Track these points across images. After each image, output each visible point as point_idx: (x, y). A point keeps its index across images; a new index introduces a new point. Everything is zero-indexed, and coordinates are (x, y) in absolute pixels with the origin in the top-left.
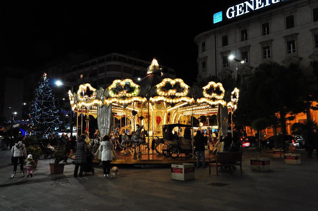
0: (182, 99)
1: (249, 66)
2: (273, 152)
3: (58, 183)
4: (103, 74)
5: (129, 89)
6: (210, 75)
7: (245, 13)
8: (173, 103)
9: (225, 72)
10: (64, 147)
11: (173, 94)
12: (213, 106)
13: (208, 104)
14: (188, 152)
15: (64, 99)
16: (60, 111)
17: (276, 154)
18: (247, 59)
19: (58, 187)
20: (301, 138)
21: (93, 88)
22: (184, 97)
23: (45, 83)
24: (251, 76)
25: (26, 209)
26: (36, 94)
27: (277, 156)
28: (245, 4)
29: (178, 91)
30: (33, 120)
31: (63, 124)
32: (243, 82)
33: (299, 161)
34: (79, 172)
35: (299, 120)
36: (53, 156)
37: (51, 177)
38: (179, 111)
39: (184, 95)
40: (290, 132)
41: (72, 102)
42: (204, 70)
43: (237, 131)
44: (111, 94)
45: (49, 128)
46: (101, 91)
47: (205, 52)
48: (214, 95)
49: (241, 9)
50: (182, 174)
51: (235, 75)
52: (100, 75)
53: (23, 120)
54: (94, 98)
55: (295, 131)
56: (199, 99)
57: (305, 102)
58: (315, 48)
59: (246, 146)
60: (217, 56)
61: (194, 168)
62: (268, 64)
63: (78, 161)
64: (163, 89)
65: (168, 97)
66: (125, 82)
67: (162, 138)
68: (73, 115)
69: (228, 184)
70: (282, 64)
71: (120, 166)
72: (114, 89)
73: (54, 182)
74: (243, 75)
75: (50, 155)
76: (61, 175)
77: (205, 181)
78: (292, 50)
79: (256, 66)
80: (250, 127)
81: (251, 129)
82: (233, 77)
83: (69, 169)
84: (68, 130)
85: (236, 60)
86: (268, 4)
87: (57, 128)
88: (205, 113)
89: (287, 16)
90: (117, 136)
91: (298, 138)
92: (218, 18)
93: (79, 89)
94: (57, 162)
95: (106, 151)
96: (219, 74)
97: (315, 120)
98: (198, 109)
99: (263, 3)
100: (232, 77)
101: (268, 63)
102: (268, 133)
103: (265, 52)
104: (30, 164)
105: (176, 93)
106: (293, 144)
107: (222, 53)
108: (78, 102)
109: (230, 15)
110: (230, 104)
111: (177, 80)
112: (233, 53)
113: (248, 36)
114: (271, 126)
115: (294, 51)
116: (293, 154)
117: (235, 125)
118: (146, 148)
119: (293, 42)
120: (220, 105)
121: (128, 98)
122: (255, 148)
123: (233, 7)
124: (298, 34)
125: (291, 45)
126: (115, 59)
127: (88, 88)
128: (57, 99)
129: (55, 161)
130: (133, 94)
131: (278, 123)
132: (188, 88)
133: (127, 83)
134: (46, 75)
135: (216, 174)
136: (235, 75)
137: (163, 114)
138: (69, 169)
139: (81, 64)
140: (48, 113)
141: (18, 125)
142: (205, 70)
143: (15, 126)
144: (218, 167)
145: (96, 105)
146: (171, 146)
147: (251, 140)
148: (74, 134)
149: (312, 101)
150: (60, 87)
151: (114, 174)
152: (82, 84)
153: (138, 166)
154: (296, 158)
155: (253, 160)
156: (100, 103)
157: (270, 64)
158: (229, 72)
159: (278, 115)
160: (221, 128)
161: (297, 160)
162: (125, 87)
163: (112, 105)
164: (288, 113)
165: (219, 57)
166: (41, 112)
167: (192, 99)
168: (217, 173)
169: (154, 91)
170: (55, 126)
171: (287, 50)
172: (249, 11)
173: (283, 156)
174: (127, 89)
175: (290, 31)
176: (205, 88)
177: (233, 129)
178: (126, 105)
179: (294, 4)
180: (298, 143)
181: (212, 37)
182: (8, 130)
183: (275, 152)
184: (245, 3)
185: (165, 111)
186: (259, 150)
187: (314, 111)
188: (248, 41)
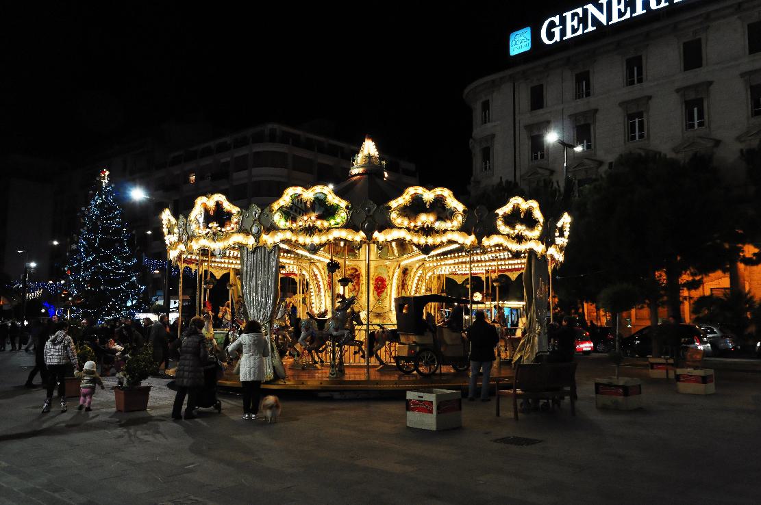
0: (450, 236)
2: (650, 365)
4: (244, 174)
6: (501, 178)
7: (585, 31)
8: (427, 245)
11: (428, 225)
12: (517, 255)
13: (506, 249)
14: (459, 362)
15: (149, 232)
16: (140, 260)
17: (655, 371)
18: (589, 141)
20: (715, 333)
21: (232, 205)
22: (452, 233)
25: (57, 495)
27: (657, 373)
28: (587, 9)
29: (439, 218)
30: (74, 281)
33: (711, 388)
34: (184, 407)
37: (118, 420)
38: (427, 265)
39: (453, 227)
40: (690, 316)
41: (169, 239)
44: (278, 219)
46: (253, 213)
47: (489, 125)
48: (520, 228)
49: (575, 23)
51: (560, 181)
52: (236, 175)
53: (51, 282)
54: (235, 229)
56: (488, 237)
58: (752, 117)
59: (585, 349)
60: (517, 132)
61: (459, 401)
62: (640, 155)
63: (185, 380)
65: (417, 232)
66: (313, 193)
67: (396, 327)
68: (170, 272)
70: (673, 155)
71: (284, 395)
73: (125, 430)
74: (579, 181)
76: (140, 414)
78: (696, 122)
79: (611, 158)
80: (594, 305)
81: (598, 309)
82: (555, 185)
83: (161, 396)
84: (159, 305)
85: (565, 145)
86: (640, 11)
88: (481, 272)
90: (285, 322)
92: (520, 43)
95: (252, 358)
96: (521, 177)
98: (479, 259)
99: (629, 8)
100: (553, 183)
101: (639, 151)
102: (637, 318)
103: (633, 125)
104: (90, 381)
105: (435, 222)
106: (696, 347)
107: (529, 128)
108: (191, 237)
109: (550, 35)
110: (552, 251)
111: (439, 191)
112: (556, 127)
113: (591, 87)
114: (645, 303)
115: (701, 124)
116: (696, 371)
117: (559, 299)
118: (355, 353)
119: (699, 103)
120: (532, 252)
121: (320, 231)
122: (606, 354)
123: (558, 16)
124: (711, 83)
125: (696, 110)
126: (273, 138)
127: (218, 205)
128: (134, 232)
130: (332, 222)
131: (662, 296)
132: (464, 211)
134: (107, 173)
135: (511, 415)
136: (560, 181)
137: (391, 274)
138: (161, 396)
140: (111, 265)
142: (489, 167)
143: (30, 296)
144: (518, 400)
145: (241, 247)
146: (418, 349)
147: (597, 335)
149: (744, 243)
150: (140, 203)
151: (268, 413)
152: (204, 194)
154: (704, 380)
155: (601, 384)
156: (250, 241)
157: (643, 154)
158: (547, 173)
159: (662, 276)
160: (533, 308)
163: (280, 249)
164: (686, 272)
166: (93, 263)
167: (472, 238)
170: (127, 298)
172: (595, 28)
173: (672, 375)
174: (318, 210)
176: (500, 212)
177: (554, 309)
178: (315, 248)
179: (703, 11)
180: (709, 345)
181: (507, 88)
183: (652, 366)
184: (585, 7)
185: (396, 263)
187: (748, 267)
188: (591, 99)
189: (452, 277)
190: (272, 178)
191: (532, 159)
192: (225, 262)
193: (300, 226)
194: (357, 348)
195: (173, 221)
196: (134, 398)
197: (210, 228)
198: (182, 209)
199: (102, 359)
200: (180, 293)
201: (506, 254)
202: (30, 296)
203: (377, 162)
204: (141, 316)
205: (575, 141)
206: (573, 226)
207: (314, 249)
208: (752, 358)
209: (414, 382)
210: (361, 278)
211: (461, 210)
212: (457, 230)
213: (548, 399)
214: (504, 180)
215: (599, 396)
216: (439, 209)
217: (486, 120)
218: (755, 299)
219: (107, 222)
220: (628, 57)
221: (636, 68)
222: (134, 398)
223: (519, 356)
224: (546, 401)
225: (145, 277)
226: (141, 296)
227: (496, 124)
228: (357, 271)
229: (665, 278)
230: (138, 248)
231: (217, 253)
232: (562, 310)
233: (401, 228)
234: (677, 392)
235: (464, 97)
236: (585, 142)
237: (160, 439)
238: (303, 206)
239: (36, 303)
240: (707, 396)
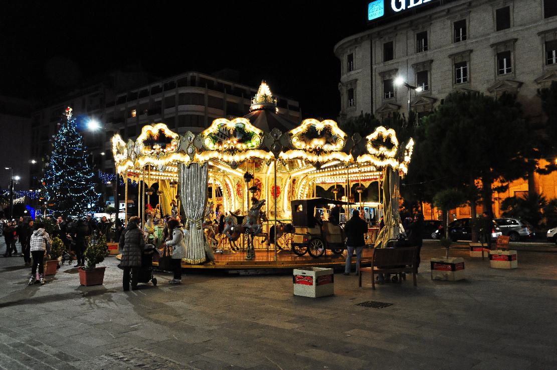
0: (334, 155)
1: (430, 96)
3: (94, 303)
4: (173, 109)
5: (242, 135)
6: (362, 112)
9: (387, 108)
11: (319, 148)
12: (380, 169)
15: (103, 154)
17: (475, 252)
20: (517, 224)
21: (172, 132)
22: (336, 153)
23: (70, 124)
24: (433, 115)
25: (36, 348)
26: (54, 144)
27: (477, 254)
29: (327, 142)
32: (419, 125)
33: (515, 264)
35: (515, 192)
37: (81, 292)
40: (499, 212)
41: (117, 158)
42: (351, 104)
43: (407, 210)
44: (208, 143)
45: (78, 205)
46: (189, 138)
47: (352, 72)
48: (383, 150)
50: (310, 287)
51: (405, 113)
53: (31, 191)
55: (507, 211)
61: (332, 276)
62: (464, 94)
63: (131, 262)
64: (303, 138)
65: (311, 152)
66: (235, 123)
67: (289, 222)
69: (392, 304)
73: (87, 299)
76: (98, 288)
77: (352, 299)
79: (443, 96)
80: (430, 205)
81: (432, 207)
82: (402, 116)
85: (409, 87)
89: (497, 9)
91: (513, 222)
96: (376, 111)
97: (543, 191)
100: (400, 115)
101: (463, 91)
102: (462, 212)
103: (459, 71)
107: (383, 74)
113: (428, 44)
114: (466, 203)
115: (508, 71)
117: (404, 201)
118: (263, 242)
119: (507, 55)
120: (389, 168)
121: (240, 151)
124: (516, 40)
125: (505, 60)
126: (193, 83)
128: (91, 154)
130: (249, 145)
132: (345, 137)
135: (370, 285)
136: (405, 113)
137: (284, 181)
139: (134, 91)
140: (75, 178)
145: (179, 164)
146: (310, 238)
148: (122, 216)
149: (539, 158)
154: (510, 258)
156: (186, 159)
157: (466, 93)
158: (395, 108)
161: (512, 262)
162: (235, 131)
165: (378, 82)
166: (62, 176)
169: (288, 141)
170: (88, 201)
171: (496, 69)
174: (239, 136)
175: (503, 35)
181: (366, 45)
183: (472, 249)
185: (287, 175)
186: (446, 244)
188: (428, 52)
189: (321, 185)
190: (194, 113)
191: (384, 98)
192: (374, 175)
193: (225, 148)
195: (123, 143)
196: (94, 277)
197: (154, 149)
198: (130, 134)
199: (70, 247)
201: (372, 168)
202: (17, 200)
203: (271, 101)
204: (98, 216)
205: (417, 83)
206: (415, 148)
207: (235, 166)
208: (543, 242)
209: (304, 262)
211: (343, 137)
213: (396, 274)
214: (364, 113)
215: (433, 270)
216: (327, 135)
218: (546, 199)
219: (71, 147)
220: (456, 21)
221: (461, 30)
223: (380, 242)
224: (395, 275)
225: (101, 187)
227: (358, 71)
228: (259, 181)
231: (159, 168)
233: (300, 150)
234: (490, 267)
235: (335, 51)
236: (424, 85)
237: (112, 306)
240: (512, 270)
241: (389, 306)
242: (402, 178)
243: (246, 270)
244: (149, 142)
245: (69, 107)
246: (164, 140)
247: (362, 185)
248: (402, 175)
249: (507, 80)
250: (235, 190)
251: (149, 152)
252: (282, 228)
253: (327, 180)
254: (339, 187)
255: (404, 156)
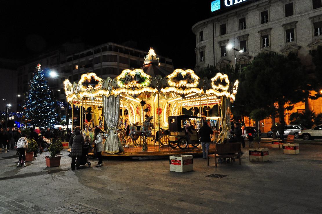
0: (192, 90)
1: (247, 55)
3: (55, 177)
4: (99, 64)
6: (208, 64)
8: (183, 94)
9: (223, 62)
10: (60, 139)
11: (184, 86)
12: (219, 97)
13: (215, 95)
15: (59, 91)
16: (55, 102)
17: (274, 145)
18: (245, 48)
19: (54, 180)
20: (299, 128)
22: (193, 88)
23: (40, 74)
24: (249, 66)
25: (21, 204)
27: (276, 146)
29: (188, 82)
31: (58, 116)
32: (241, 72)
33: (298, 151)
36: (49, 149)
37: (47, 171)
40: (289, 121)
41: (67, 93)
42: (202, 60)
44: (120, 84)
45: (45, 121)
46: (109, 81)
47: (203, 42)
48: (221, 86)
51: (233, 65)
52: (95, 65)
53: (18, 113)
55: (293, 121)
57: (304, 91)
60: (215, 45)
65: (179, 88)
66: (135, 72)
67: (167, 129)
72: (122, 79)
73: (51, 175)
75: (46, 148)
76: (57, 168)
78: (291, 39)
79: (254, 55)
80: (248, 118)
81: (250, 119)
82: (231, 67)
83: (66, 160)
84: (64, 122)
85: (235, 50)
87: (53, 121)
88: (197, 105)
91: (296, 127)
93: (81, 78)
94: (53, 155)
100: (230, 66)
107: (220, 43)
114: (270, 116)
115: (293, 40)
117: (234, 116)
118: (152, 140)
119: (292, 31)
120: (224, 97)
121: (138, 88)
124: (297, 22)
125: (290, 33)
126: (111, 49)
127: (92, 78)
128: (52, 91)
129: (51, 155)
130: (143, 84)
131: (277, 113)
132: (199, 79)
133: (137, 73)
134: (40, 65)
135: (214, 165)
136: (233, 65)
137: (164, 105)
140: (43, 105)
141: (13, 117)
143: (9, 119)
145: (103, 96)
146: (179, 138)
148: (71, 126)
152: (86, 73)
153: (136, 158)
154: (295, 148)
155: (252, 151)
156: (107, 93)
158: (227, 62)
159: (276, 105)
161: (296, 150)
162: (135, 77)
166: (35, 104)
168: (216, 165)
170: (51, 119)
171: (286, 39)
173: (281, 146)
174: (137, 79)
181: (210, 26)
182: (2, 122)
188: (247, 30)
191: (221, 56)
193: (129, 87)
194: (153, 138)
195: (70, 85)
196: (54, 162)
197: (89, 88)
198: (75, 79)
200: (73, 116)
201: (215, 97)
204: (57, 126)
206: (239, 85)
207: (135, 97)
209: (176, 152)
210: (151, 108)
211: (197, 79)
212: (196, 87)
214: (210, 65)
215: (251, 156)
216: (188, 78)
217: (201, 40)
219: (41, 87)
222: (54, 162)
224: (228, 158)
226: (57, 118)
228: (149, 105)
229: (278, 105)
230: (55, 98)
231: (92, 98)
232: (235, 120)
236: (244, 48)
237: (65, 178)
238: (131, 78)
239: (12, 122)
240: (296, 155)
241: (225, 176)
242: (232, 102)
243: (142, 157)
244: (86, 84)
245: (39, 64)
246: (94, 82)
247: (209, 107)
248: (232, 101)
249: (293, 45)
250: (136, 111)
251: (85, 89)
252: (163, 133)
253: (189, 104)
254: (196, 108)
255: (233, 90)
